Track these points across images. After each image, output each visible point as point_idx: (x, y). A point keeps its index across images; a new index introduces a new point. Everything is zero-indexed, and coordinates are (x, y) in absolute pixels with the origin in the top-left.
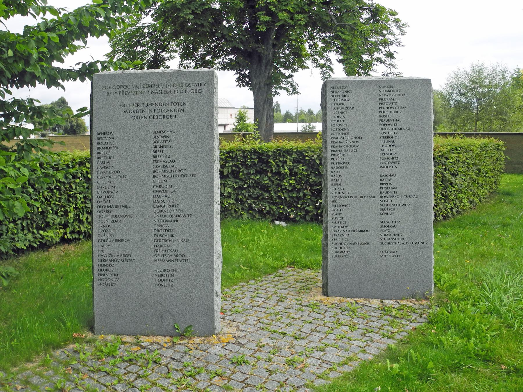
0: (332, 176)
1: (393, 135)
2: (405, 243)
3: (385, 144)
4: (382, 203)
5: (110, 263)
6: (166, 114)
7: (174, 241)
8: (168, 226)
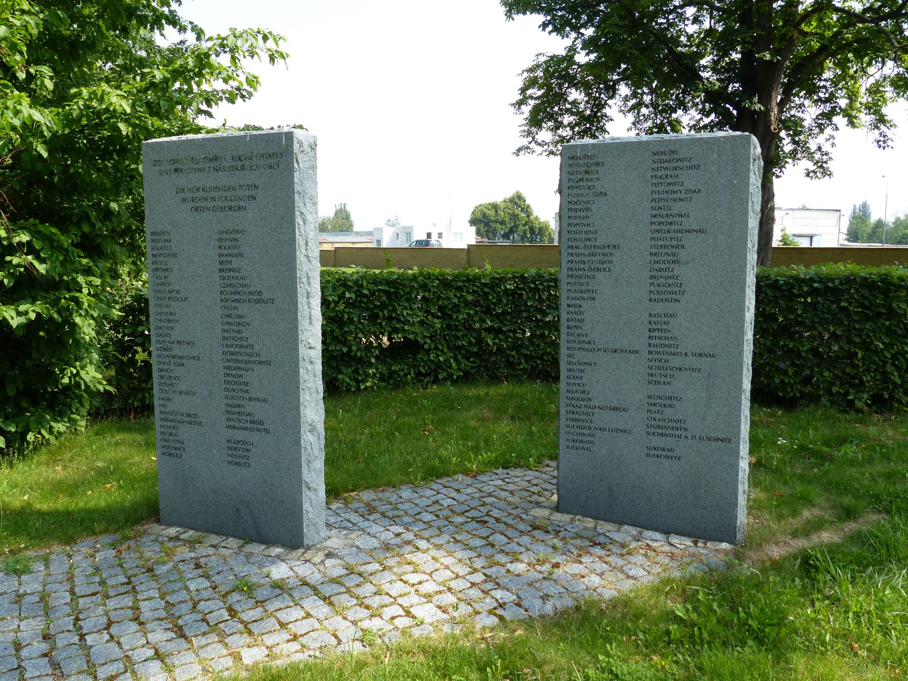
0: (568, 313)
1: (674, 243)
2: (690, 437)
3: (661, 258)
4: (651, 364)
5: (174, 424)
6: (233, 204)
7: (250, 399)
8: (240, 376)
